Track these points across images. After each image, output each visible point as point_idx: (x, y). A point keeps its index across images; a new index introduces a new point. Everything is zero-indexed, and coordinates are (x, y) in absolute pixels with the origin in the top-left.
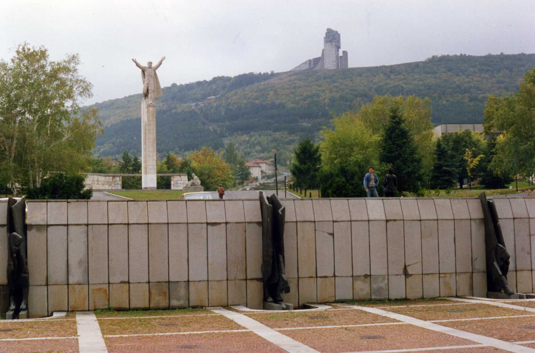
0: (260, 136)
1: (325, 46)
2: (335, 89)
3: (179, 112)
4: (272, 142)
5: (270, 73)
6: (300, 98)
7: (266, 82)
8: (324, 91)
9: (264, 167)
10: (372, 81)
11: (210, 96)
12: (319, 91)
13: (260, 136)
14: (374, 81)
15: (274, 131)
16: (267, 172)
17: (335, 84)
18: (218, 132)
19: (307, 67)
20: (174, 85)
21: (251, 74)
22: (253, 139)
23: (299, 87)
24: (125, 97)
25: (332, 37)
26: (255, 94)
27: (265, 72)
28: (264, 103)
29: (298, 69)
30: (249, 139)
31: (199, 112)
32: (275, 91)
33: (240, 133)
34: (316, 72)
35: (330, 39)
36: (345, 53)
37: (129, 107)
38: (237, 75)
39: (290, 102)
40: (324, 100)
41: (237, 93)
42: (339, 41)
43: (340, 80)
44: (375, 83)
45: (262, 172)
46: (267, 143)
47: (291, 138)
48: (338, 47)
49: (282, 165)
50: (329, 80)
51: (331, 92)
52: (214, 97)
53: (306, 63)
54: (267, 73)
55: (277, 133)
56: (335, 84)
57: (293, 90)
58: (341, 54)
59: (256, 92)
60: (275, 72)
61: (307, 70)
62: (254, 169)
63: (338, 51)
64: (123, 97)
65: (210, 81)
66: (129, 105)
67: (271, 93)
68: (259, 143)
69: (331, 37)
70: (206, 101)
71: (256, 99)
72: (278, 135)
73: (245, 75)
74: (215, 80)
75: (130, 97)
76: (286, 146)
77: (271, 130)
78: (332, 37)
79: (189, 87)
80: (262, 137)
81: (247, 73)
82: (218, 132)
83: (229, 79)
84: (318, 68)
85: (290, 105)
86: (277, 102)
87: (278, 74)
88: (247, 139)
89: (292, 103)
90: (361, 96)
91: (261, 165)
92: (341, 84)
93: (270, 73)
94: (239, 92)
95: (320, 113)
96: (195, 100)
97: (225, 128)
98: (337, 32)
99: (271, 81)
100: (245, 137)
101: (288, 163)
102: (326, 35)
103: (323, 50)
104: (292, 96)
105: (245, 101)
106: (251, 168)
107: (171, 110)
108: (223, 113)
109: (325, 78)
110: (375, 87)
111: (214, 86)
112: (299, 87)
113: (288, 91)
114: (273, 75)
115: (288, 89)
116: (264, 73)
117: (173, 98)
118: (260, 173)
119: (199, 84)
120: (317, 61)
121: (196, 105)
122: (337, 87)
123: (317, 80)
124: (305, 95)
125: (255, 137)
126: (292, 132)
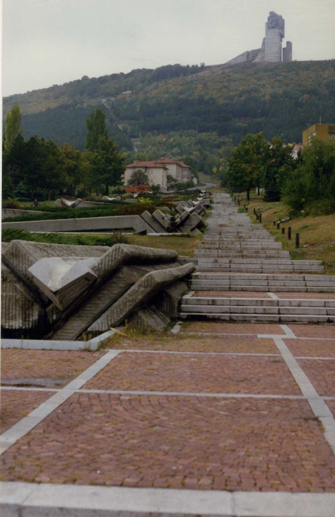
0: (181, 136)
1: (267, 33)
2: (277, 84)
3: (85, 107)
4: (196, 144)
5: (199, 66)
6: (234, 93)
7: (194, 75)
8: (264, 85)
9: (173, 170)
10: (321, 76)
11: (126, 90)
12: (258, 85)
13: (181, 136)
14: (323, 76)
15: (200, 132)
16: (179, 178)
17: (278, 78)
18: (129, 130)
19: (245, 59)
20: (85, 78)
21: (178, 66)
22: (172, 140)
23: (234, 81)
24: (28, 92)
25: (275, 23)
26: (181, 88)
27: (195, 64)
28: (189, 98)
29: (234, 62)
30: (167, 140)
31: (110, 108)
32: (205, 85)
33: (156, 132)
34: (255, 64)
35: (273, 25)
36: (289, 44)
37: (29, 102)
38: (159, 65)
39: (222, 98)
40: (264, 96)
41: (158, 86)
42: (282, 28)
43: (283, 73)
44: (325, 79)
45: (169, 178)
46: (189, 146)
47: (221, 140)
48: (282, 36)
49: (206, 173)
50: (271, 73)
51: (272, 87)
52: (130, 92)
53: (243, 55)
54: (197, 66)
55: (204, 134)
56: (278, 78)
57: (226, 84)
58: (284, 45)
59: (181, 85)
60: (206, 65)
61: (245, 62)
62: (154, 171)
63: (281, 41)
64: (26, 92)
65: (128, 74)
66: (30, 100)
67: (200, 86)
68: (179, 145)
69: (274, 23)
70: (119, 97)
71: (181, 94)
72: (204, 136)
73: (169, 67)
74: (134, 72)
75: (34, 92)
76: (214, 150)
77: (195, 129)
78: (275, 23)
79: (103, 80)
80: (184, 137)
81: (173, 64)
82: (129, 130)
83: (150, 71)
84: (257, 60)
85: (221, 101)
86: (206, 98)
87: (209, 67)
88: (164, 140)
89: (224, 99)
90: (308, 93)
91: (168, 166)
92: (285, 77)
93: (199, 66)
94: (160, 85)
95: (260, 111)
96: (108, 95)
97: (137, 127)
98: (281, 17)
99: (200, 74)
100: (161, 138)
101: (215, 170)
102: (269, 19)
103: (264, 39)
104: (225, 90)
105: (167, 96)
106: (150, 170)
107: (76, 105)
108: (138, 110)
109: (265, 71)
110: (325, 82)
111: (131, 79)
112: (234, 81)
113: (220, 84)
114: (203, 68)
115: (220, 82)
116: (193, 66)
117: (82, 93)
118: (166, 180)
119: (114, 76)
120: (255, 53)
121: (107, 101)
122: (280, 81)
123: (255, 73)
124: (241, 89)
125: (175, 137)
126: (223, 132)
